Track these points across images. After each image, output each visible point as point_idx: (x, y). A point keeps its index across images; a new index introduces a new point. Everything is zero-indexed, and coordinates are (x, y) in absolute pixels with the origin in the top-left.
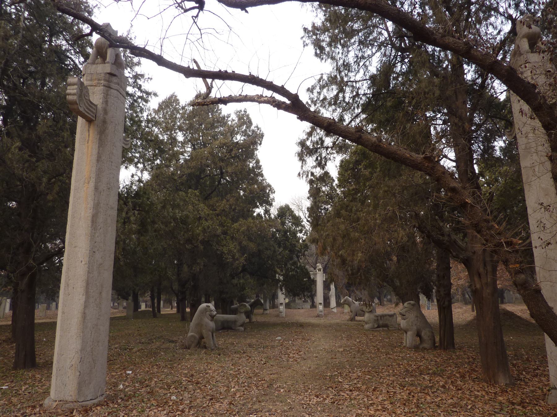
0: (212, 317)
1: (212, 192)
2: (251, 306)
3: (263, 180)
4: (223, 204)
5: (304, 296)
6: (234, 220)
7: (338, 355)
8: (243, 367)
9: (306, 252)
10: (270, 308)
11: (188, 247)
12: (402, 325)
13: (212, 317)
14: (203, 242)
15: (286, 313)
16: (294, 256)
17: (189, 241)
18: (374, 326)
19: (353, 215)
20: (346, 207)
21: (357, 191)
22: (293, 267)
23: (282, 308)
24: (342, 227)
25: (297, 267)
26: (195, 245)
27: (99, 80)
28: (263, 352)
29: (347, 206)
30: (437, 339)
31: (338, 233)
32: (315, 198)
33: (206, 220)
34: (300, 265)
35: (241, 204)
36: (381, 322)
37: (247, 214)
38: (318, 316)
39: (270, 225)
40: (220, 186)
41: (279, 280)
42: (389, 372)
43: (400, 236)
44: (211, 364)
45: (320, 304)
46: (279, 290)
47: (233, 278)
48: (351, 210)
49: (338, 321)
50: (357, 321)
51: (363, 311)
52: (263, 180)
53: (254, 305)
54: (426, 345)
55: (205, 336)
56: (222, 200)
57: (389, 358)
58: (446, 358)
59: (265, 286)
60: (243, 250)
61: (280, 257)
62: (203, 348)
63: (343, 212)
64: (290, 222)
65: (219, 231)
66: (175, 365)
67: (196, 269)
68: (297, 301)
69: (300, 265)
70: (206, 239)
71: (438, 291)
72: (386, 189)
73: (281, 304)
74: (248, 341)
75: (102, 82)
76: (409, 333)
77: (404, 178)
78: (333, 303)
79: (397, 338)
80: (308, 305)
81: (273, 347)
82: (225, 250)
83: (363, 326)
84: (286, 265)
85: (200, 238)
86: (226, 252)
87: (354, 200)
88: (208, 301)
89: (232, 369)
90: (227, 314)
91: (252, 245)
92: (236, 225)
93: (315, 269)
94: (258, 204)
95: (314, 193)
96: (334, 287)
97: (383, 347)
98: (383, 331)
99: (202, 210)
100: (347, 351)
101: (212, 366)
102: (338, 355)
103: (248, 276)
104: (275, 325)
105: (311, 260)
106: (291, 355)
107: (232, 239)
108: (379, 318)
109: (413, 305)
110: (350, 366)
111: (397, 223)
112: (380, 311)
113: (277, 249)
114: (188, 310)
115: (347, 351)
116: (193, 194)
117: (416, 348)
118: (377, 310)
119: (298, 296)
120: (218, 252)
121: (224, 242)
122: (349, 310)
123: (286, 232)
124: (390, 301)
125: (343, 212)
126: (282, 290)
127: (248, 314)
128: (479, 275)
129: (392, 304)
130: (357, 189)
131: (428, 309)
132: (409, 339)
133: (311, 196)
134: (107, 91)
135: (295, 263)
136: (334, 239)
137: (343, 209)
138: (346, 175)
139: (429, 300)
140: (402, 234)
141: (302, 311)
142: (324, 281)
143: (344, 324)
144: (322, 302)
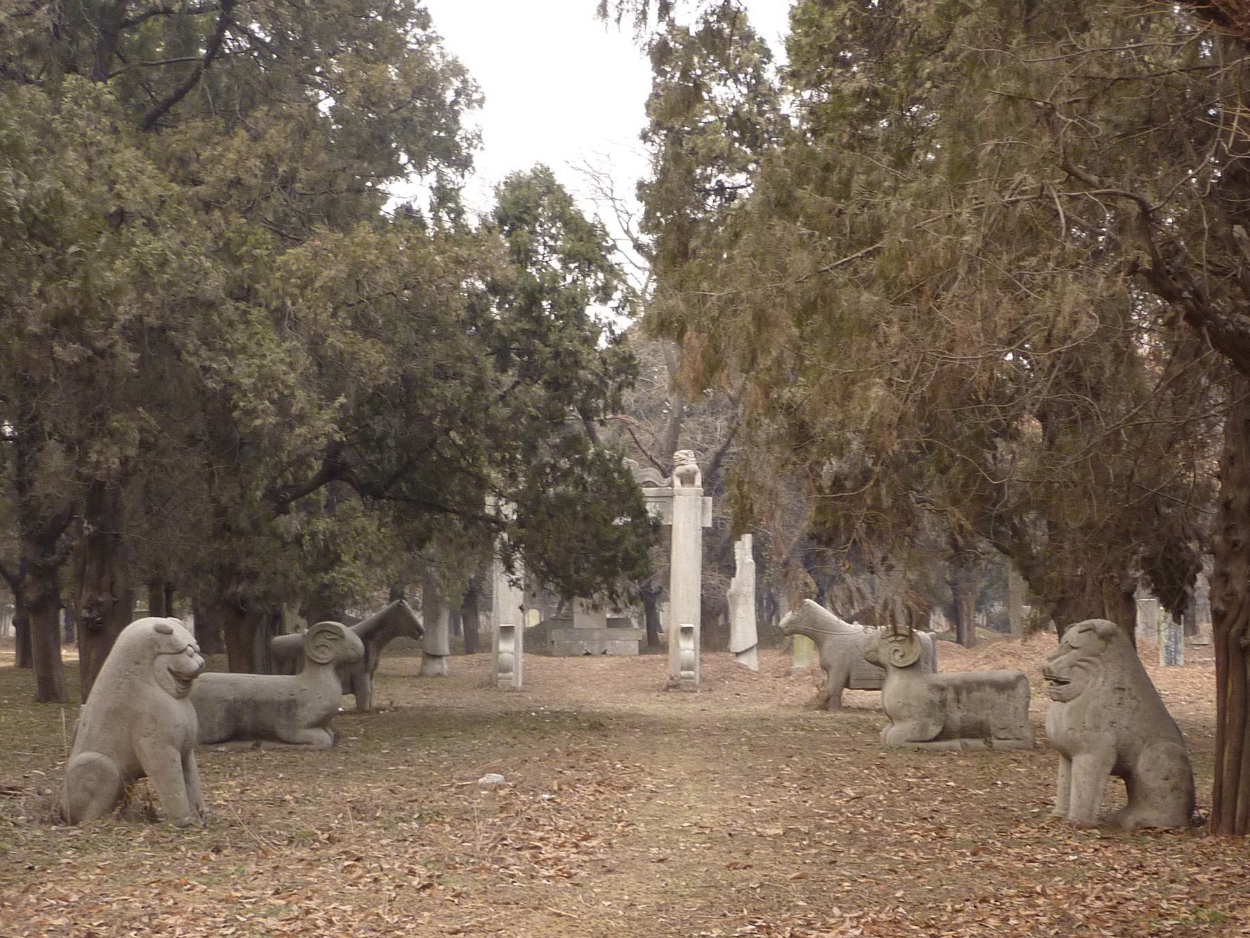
0: (185, 680)
1: (180, 95)
2: (367, 636)
3: (430, 40)
4: (232, 155)
5: (612, 593)
6: (287, 234)
7: (760, 852)
8: (327, 899)
9: (628, 396)
10: (454, 651)
11: (68, 352)
12: (1050, 728)
13: (185, 680)
14: (136, 333)
15: (527, 671)
16: (573, 415)
17: (65, 323)
18: (924, 728)
19: (853, 209)
20: (824, 174)
21: (874, 103)
22: (564, 463)
23: (508, 649)
24: (801, 261)
25: (582, 462)
26: (100, 344)
28: (418, 839)
29: (827, 168)
30: (1205, 789)
31: (781, 291)
32: (675, 139)
33: (151, 226)
34: (599, 455)
35: (323, 156)
36: (957, 716)
37: (347, 204)
38: (674, 686)
39: (458, 262)
40: (216, 65)
41: (498, 523)
42: (982, 924)
43: (1067, 309)
44: (177, 888)
45: (686, 631)
46: (498, 567)
47: (282, 509)
48: (847, 184)
49: (764, 708)
50: (848, 709)
51: (877, 663)
52: (430, 40)
53: (380, 634)
54: (1149, 815)
55: (149, 765)
56: (229, 132)
57: (989, 867)
58: (1238, 870)
59: (431, 549)
60: (329, 372)
61: (506, 412)
62: (139, 819)
63: (806, 195)
64: (553, 250)
65: (215, 283)
66: (12, 892)
67: (107, 458)
68: (582, 619)
69: (599, 455)
70: (151, 320)
71: (1221, 578)
72: (1013, 86)
73: (507, 631)
74: (353, 791)
76: (1082, 761)
77: (1100, 37)
78: (744, 629)
79: (1026, 782)
80: (630, 639)
81: (463, 816)
82: (243, 372)
83: (876, 731)
84: (531, 449)
85: (125, 311)
86: (247, 382)
87: (861, 143)
88: (160, 608)
89: (274, 911)
90: (252, 670)
91: (372, 354)
92: (296, 256)
93: (666, 473)
94: (404, 158)
95: (674, 109)
96: (749, 559)
97: (965, 820)
98: (966, 752)
99: (132, 180)
100: (803, 836)
101: (181, 896)
102: (760, 852)
103: (355, 502)
104: (473, 722)
105: (650, 434)
106: (548, 852)
107: (278, 324)
108: (950, 695)
109: (1106, 637)
110: (809, 900)
111: (1056, 251)
112: (953, 666)
113: (491, 374)
114: (70, 655)
115: (803, 836)
116: (88, 95)
117: (1109, 826)
118: (941, 664)
119: (586, 594)
120: (211, 384)
121: (240, 336)
122: (817, 660)
123: (533, 296)
124: (1002, 625)
125: (806, 195)
126: (510, 568)
127: (353, 675)
129: (1009, 640)
130: (875, 94)
131: (1171, 662)
132: (1080, 786)
133: (657, 126)
135: (572, 445)
136: (762, 320)
137: (809, 182)
138: (828, 22)
139: (1177, 620)
140: (1073, 300)
141: (598, 664)
142: (706, 532)
143: (790, 722)
144: (695, 623)
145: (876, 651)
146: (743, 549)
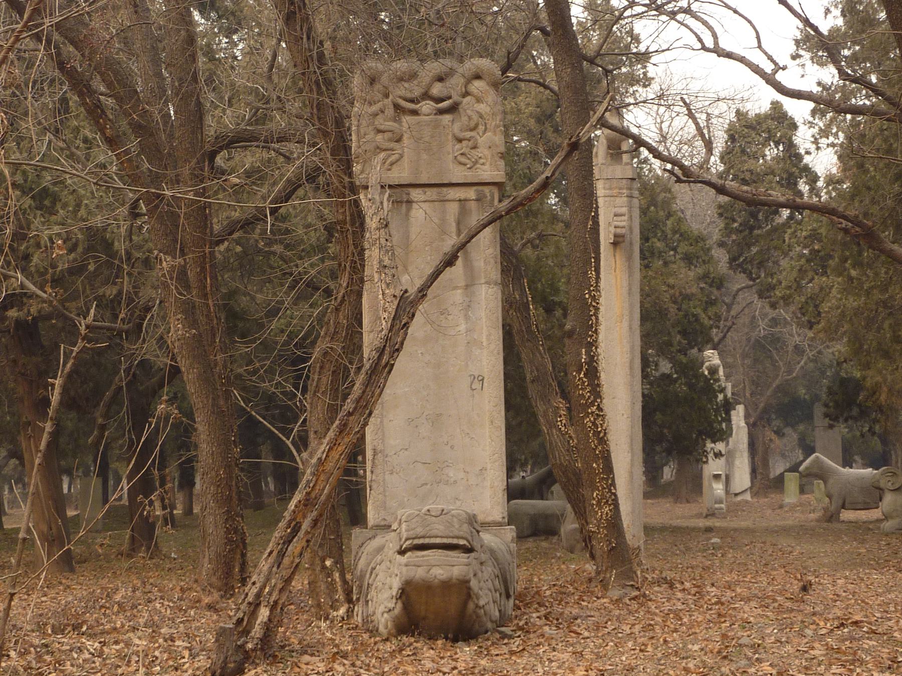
27: (620, 189)
38: (711, 514)
75: (625, 191)
128: (494, 602)
134: (630, 202)
145: (878, 481)
146: (738, 416)
